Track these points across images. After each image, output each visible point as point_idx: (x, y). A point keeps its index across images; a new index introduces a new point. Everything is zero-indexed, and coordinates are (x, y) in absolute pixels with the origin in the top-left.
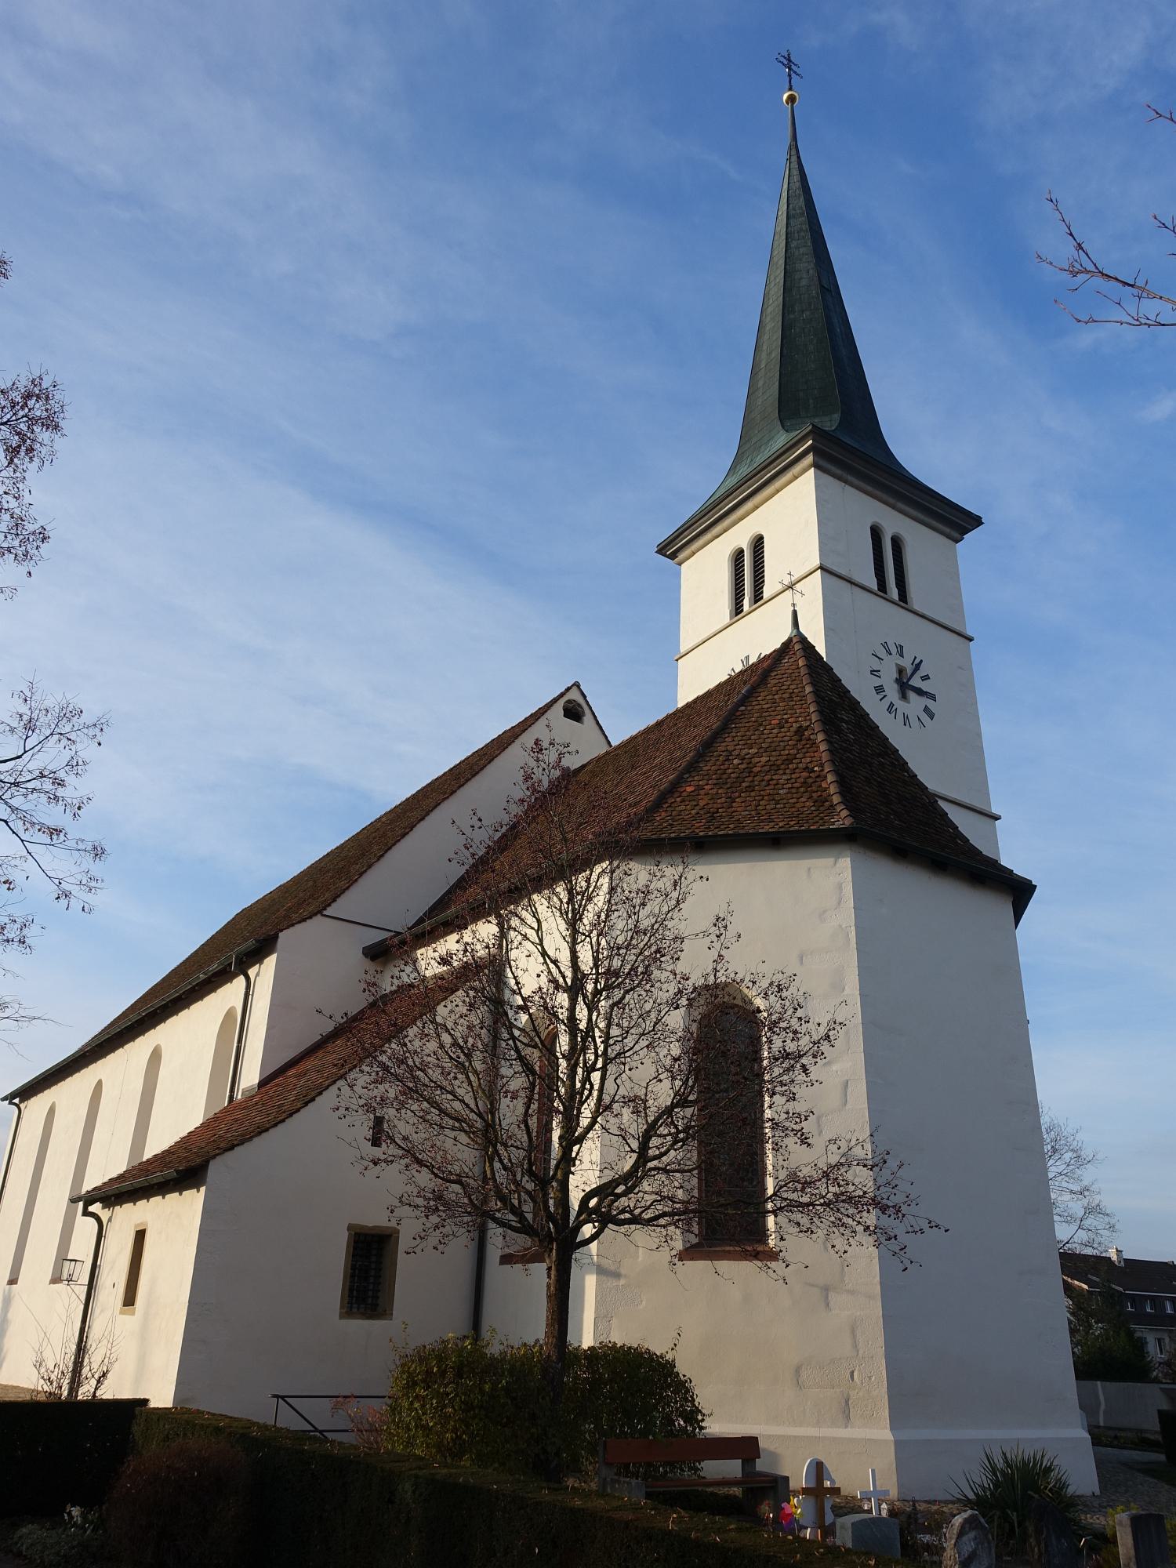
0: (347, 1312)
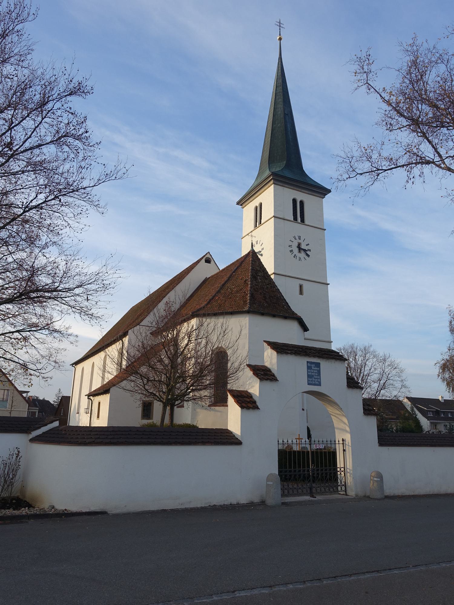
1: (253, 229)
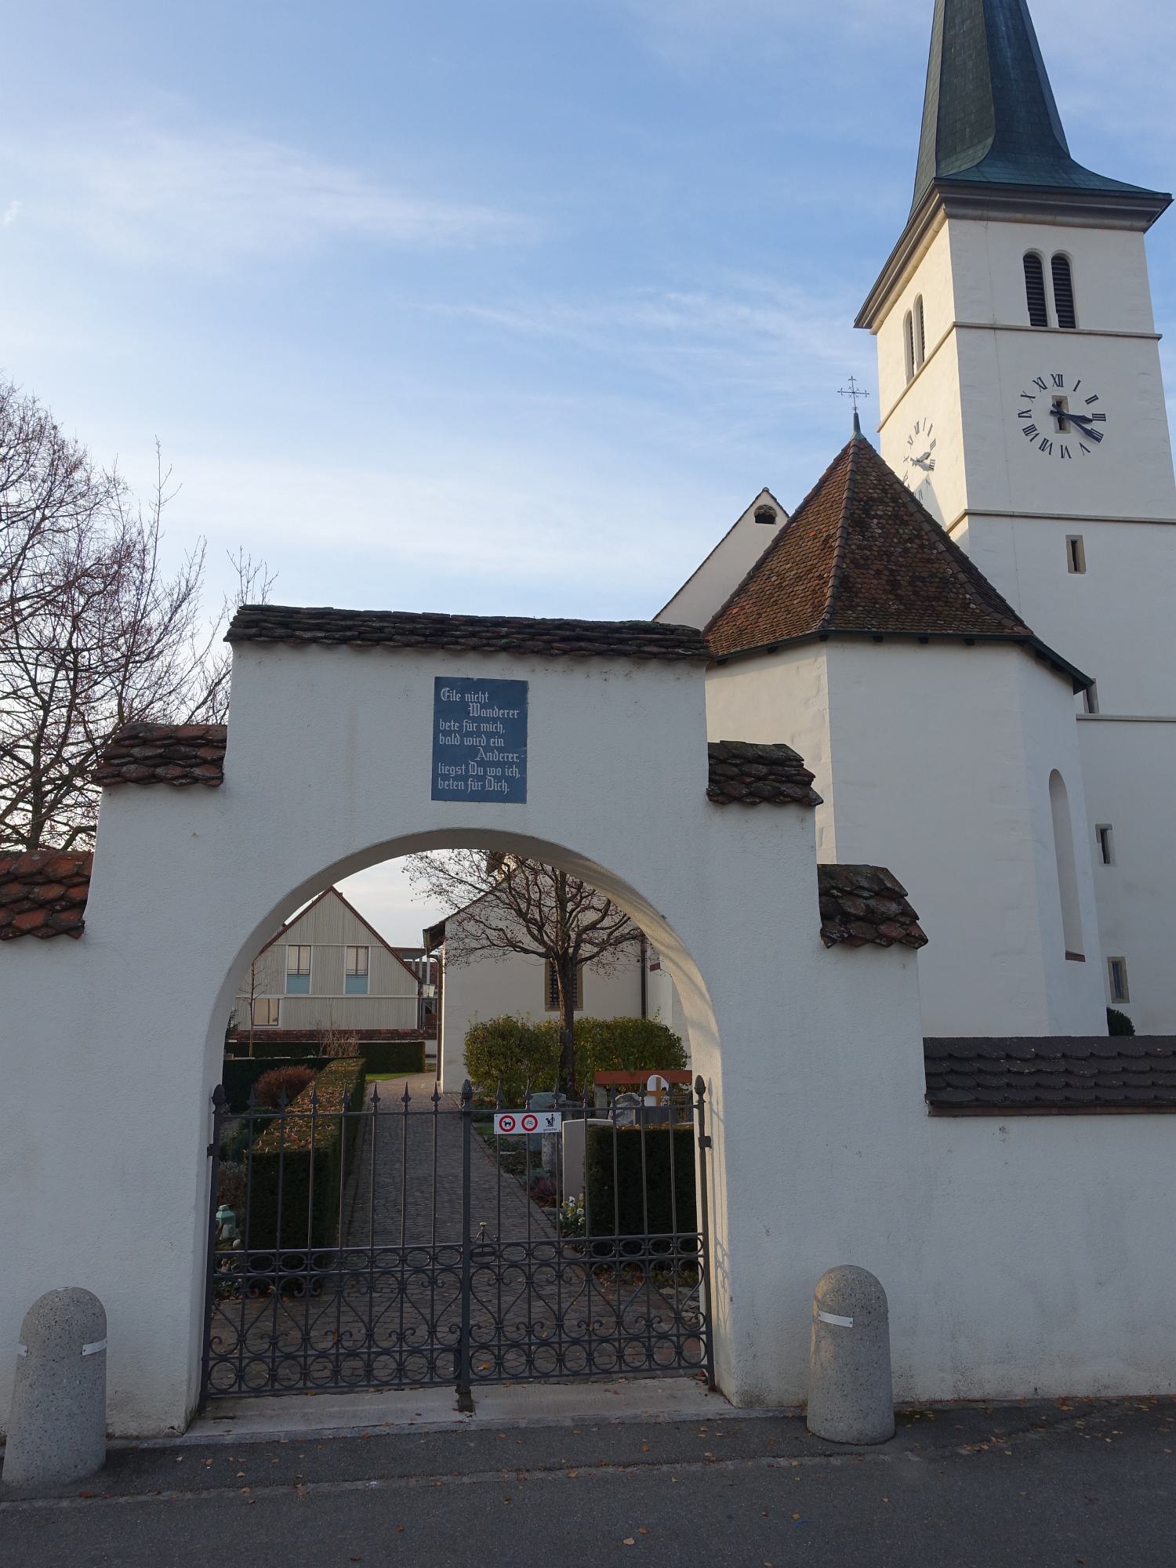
0: (549, 1008)
1: (905, 387)
